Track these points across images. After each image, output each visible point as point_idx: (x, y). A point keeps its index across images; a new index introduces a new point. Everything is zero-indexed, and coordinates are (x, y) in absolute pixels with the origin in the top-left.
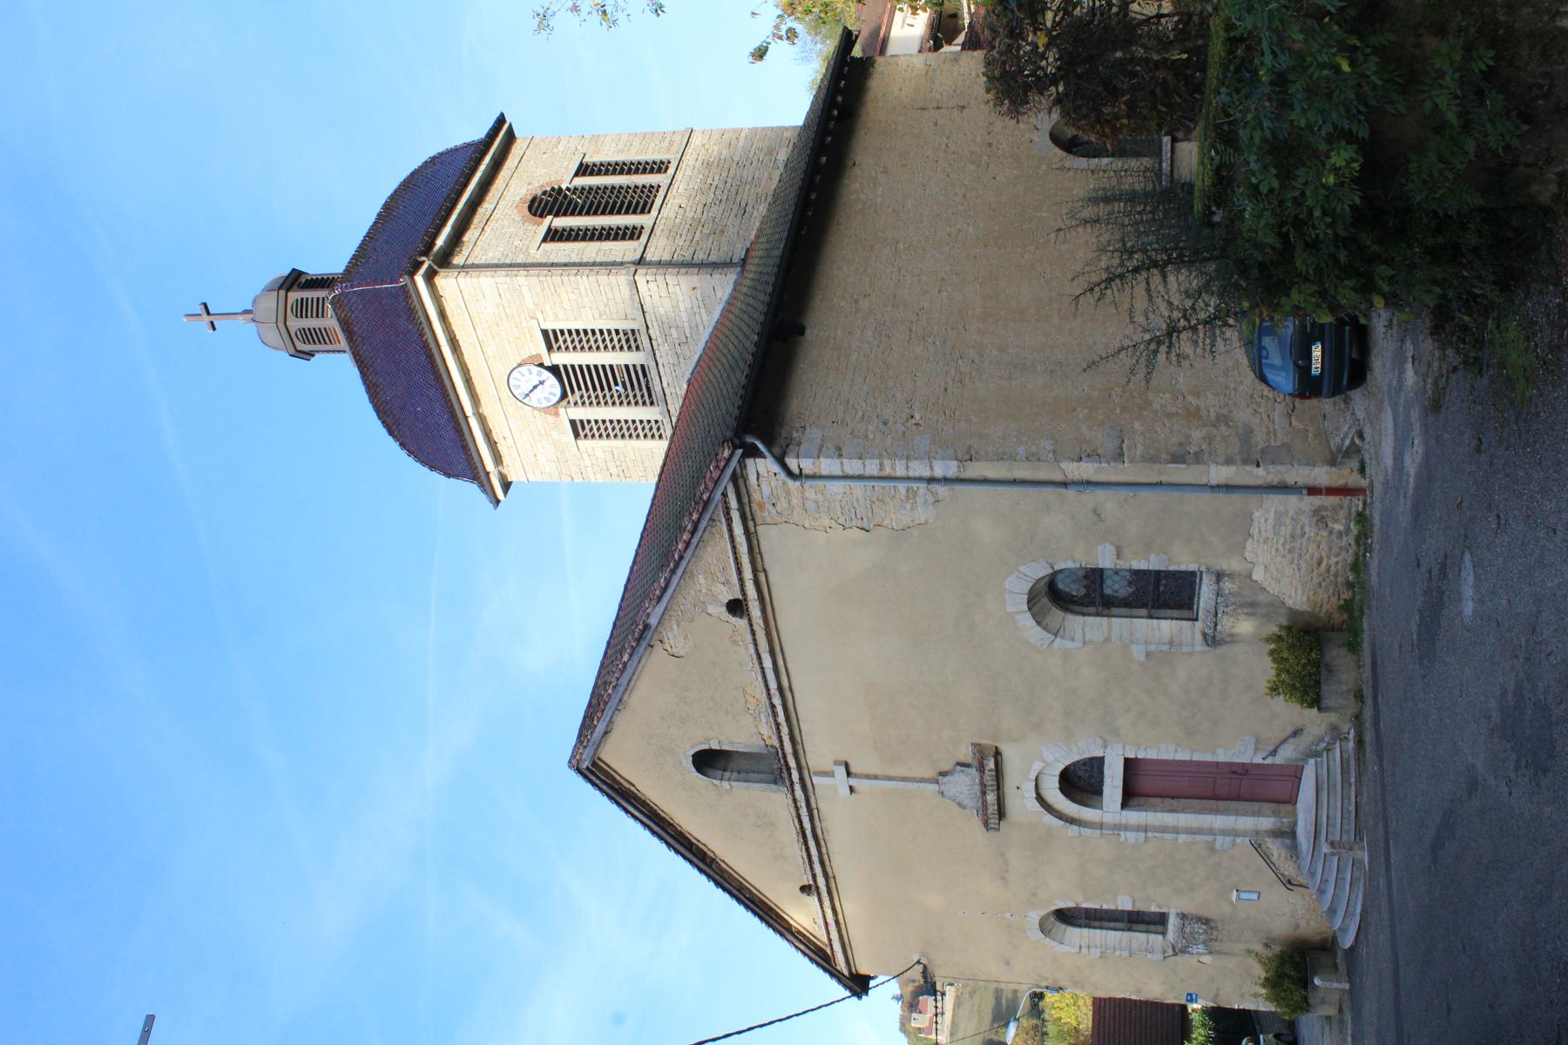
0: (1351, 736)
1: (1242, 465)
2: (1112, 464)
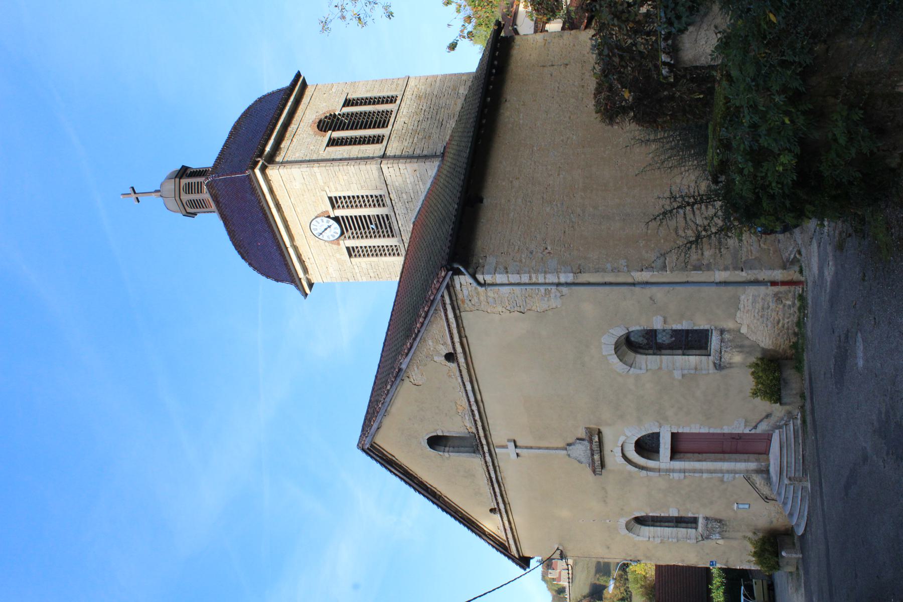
0: (799, 417)
1: (733, 271)
2: (660, 272)
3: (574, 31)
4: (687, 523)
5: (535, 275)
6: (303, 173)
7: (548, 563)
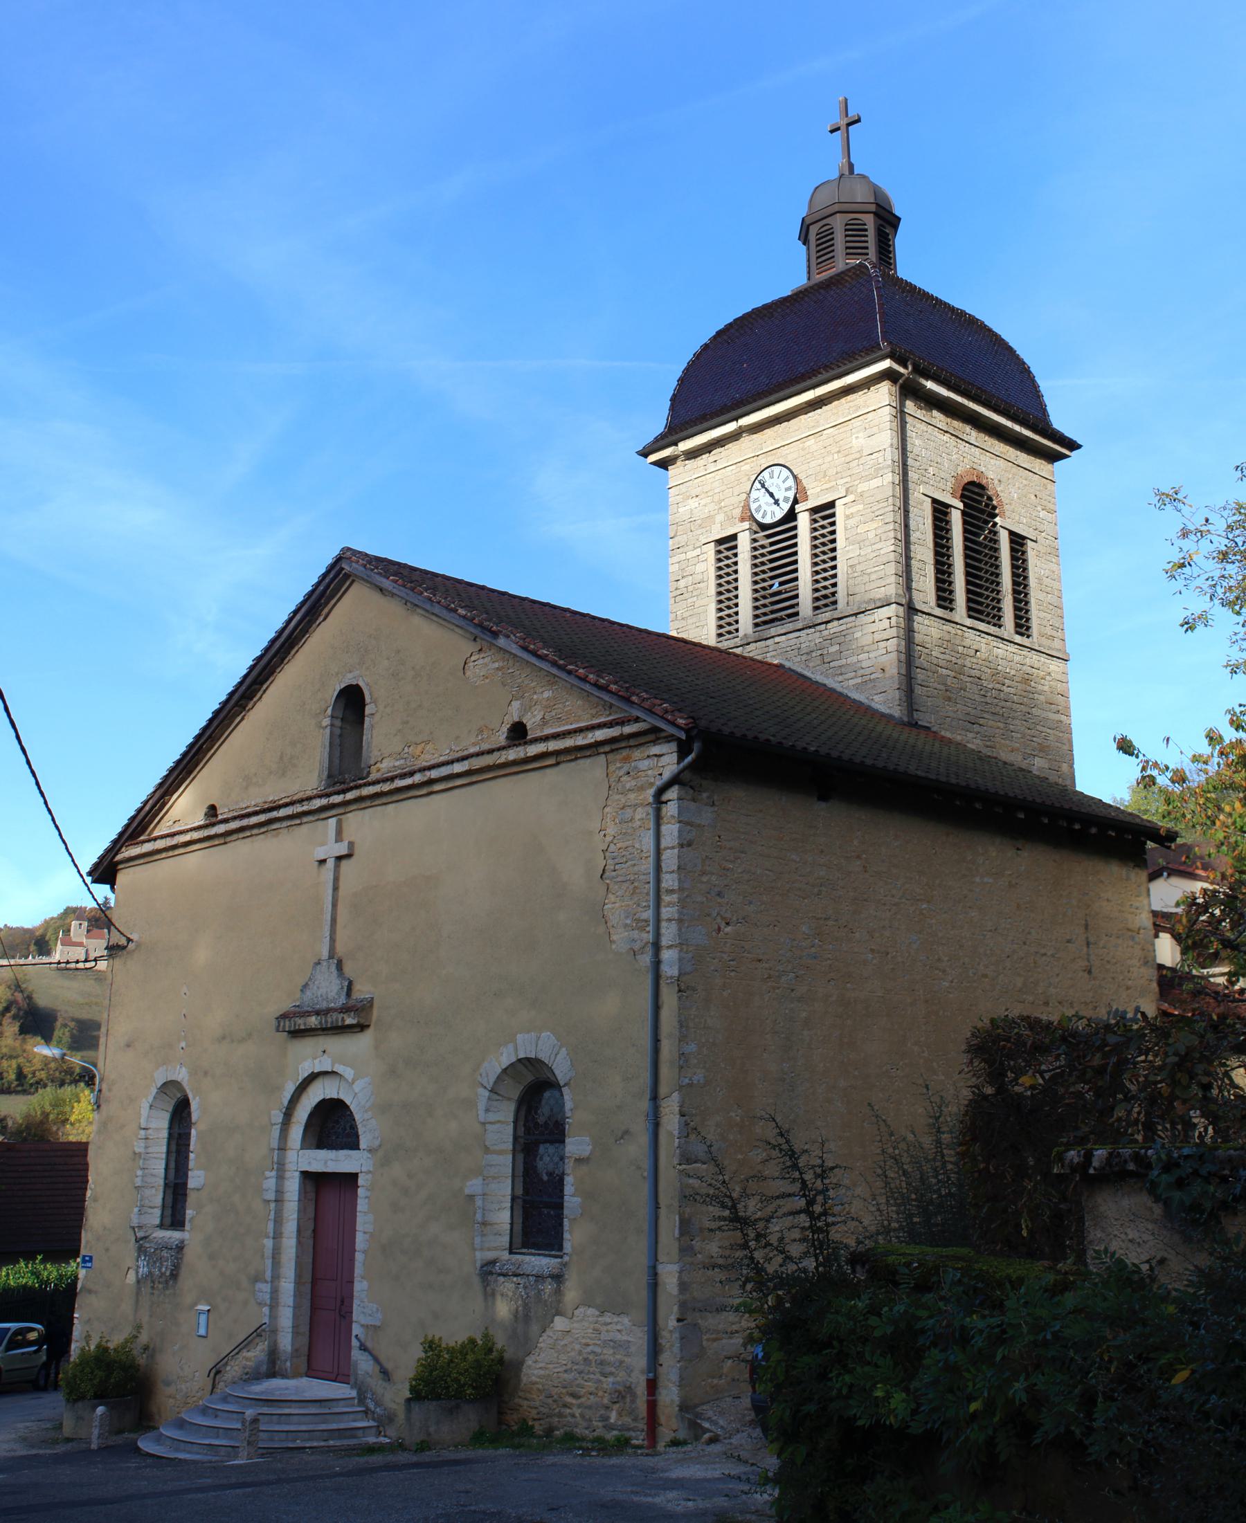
3: (1157, 989)
4: (174, 1207)
5: (676, 900)
6: (881, 454)
7: (100, 919)
